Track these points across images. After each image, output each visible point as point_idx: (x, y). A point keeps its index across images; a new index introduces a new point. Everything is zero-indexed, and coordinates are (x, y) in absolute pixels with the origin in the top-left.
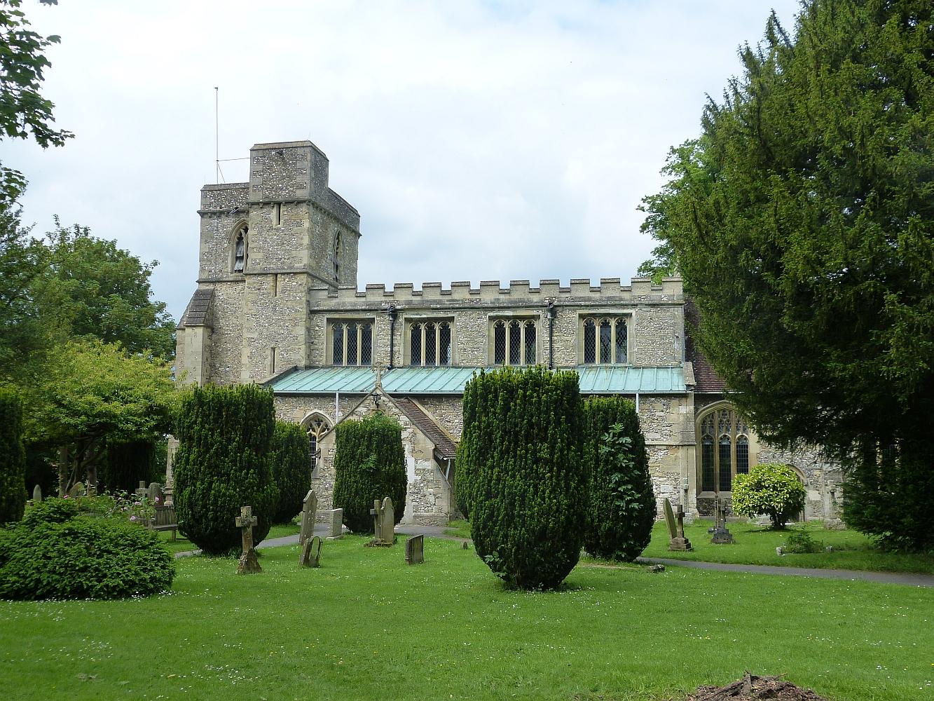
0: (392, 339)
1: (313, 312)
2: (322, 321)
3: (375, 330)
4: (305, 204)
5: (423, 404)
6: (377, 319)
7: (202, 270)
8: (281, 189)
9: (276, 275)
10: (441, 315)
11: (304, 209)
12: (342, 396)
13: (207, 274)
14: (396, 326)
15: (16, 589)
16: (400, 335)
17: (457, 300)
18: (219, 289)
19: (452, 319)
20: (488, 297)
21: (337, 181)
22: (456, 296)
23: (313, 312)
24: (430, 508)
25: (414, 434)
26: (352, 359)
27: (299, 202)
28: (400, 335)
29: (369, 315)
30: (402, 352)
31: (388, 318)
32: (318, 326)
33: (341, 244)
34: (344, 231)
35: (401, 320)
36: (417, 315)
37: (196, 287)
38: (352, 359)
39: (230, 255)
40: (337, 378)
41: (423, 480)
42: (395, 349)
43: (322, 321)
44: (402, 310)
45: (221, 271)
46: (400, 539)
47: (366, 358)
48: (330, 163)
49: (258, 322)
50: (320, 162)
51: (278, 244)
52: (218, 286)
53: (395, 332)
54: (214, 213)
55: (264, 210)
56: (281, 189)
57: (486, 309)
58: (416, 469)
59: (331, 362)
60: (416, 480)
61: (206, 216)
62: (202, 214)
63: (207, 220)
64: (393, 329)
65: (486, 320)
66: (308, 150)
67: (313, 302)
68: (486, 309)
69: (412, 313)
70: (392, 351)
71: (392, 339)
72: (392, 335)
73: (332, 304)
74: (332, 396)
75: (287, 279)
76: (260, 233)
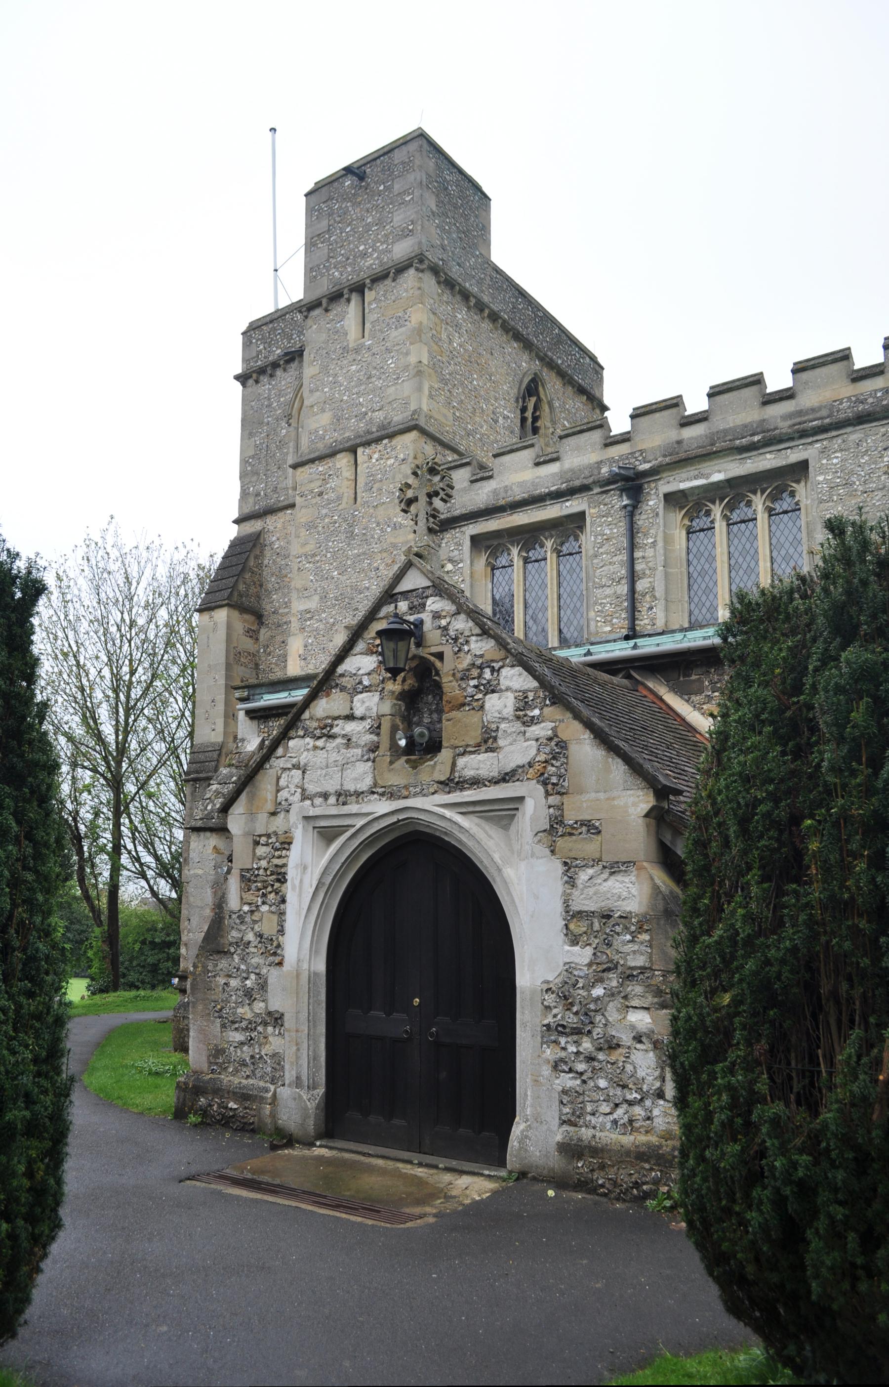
0: (632, 561)
4: (412, 271)
5: (684, 692)
6: (591, 513)
7: (244, 494)
8: (364, 255)
10: (768, 461)
13: (251, 500)
14: (642, 520)
15: (772, 1116)
16: (654, 544)
17: (813, 410)
18: (271, 528)
19: (801, 469)
21: (516, 249)
24: (638, 1110)
25: (558, 748)
27: (401, 269)
28: (654, 544)
29: (572, 506)
30: (660, 592)
31: (619, 501)
32: (450, 560)
33: (546, 407)
34: (552, 386)
35: (653, 502)
36: (696, 478)
37: (233, 531)
39: (291, 450)
41: (603, 968)
42: (641, 586)
45: (275, 490)
48: (605, 373)
49: (318, 571)
50: (461, 200)
51: (360, 383)
52: (271, 522)
53: (640, 539)
55: (331, 315)
56: (364, 255)
58: (572, 915)
60: (569, 968)
61: (251, 382)
62: (243, 378)
64: (632, 533)
66: (413, 147)
69: (684, 476)
70: (632, 591)
71: (632, 561)
72: (632, 546)
73: (483, 495)
75: (376, 456)
76: (325, 369)
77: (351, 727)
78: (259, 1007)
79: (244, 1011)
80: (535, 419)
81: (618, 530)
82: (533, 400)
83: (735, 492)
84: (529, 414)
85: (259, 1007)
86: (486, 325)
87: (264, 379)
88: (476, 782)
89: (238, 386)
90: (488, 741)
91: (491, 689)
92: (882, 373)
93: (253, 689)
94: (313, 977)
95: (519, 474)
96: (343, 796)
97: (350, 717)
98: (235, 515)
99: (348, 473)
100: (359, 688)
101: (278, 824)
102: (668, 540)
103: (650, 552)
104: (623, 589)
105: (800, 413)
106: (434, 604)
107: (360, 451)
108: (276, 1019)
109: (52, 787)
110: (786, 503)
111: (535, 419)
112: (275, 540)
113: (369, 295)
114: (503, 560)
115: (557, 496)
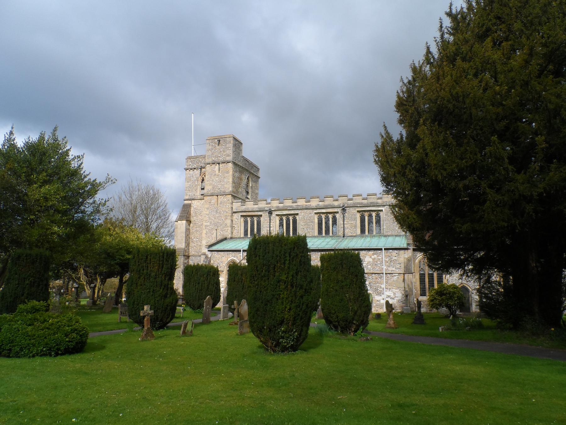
3: (262, 219)
10: (292, 212)
22: (299, 204)
26: (327, 232)
59: (242, 236)
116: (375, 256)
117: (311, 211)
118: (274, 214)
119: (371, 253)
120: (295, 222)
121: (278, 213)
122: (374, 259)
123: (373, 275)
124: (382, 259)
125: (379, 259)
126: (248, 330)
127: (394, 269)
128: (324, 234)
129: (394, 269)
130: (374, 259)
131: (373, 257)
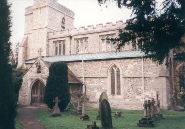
1: (49, 39)
2: (51, 42)
3: (66, 43)
6: (66, 40)
9: (39, 29)
10: (84, 36)
11: (47, 8)
12: (85, 61)
20: (99, 29)
22: (89, 30)
23: (49, 39)
26: (60, 54)
31: (49, 34)
35: (73, 39)
37: (24, 36)
38: (60, 54)
40: (128, 54)
43: (51, 42)
44: (73, 36)
46: (154, 6)
47: (64, 53)
54: (28, 14)
55: (36, 11)
57: (98, 33)
59: (54, 54)
62: (25, 15)
63: (26, 17)
65: (98, 37)
67: (49, 36)
68: (98, 33)
73: (54, 36)
74: (81, 61)
77: (34, 71)
78: (25, 94)
79: (24, 95)
80: (64, 22)
81: (74, 37)
82: (64, 20)
83: (81, 39)
84: (63, 22)
85: (25, 94)
86: (57, 12)
87: (28, 16)
88: (43, 76)
89: (24, 16)
90: (44, 73)
91: (45, 69)
92: (96, 28)
93: (26, 61)
94: (30, 92)
95: (59, 34)
96: (33, 76)
97: (34, 70)
98: (24, 14)
99: (38, 32)
100: (34, 68)
101: (27, 79)
102: (74, 44)
103: (72, 45)
104: (70, 49)
105: (88, 31)
106: (40, 61)
107: (40, 29)
108: (27, 96)
109: (53, 106)
110: (86, 41)
111: (64, 22)
112: (29, 38)
113: (41, 9)
114: (57, 44)
115: (63, 37)
116: (136, 63)
117: (96, 34)
118: (73, 38)
119: (133, 61)
120: (64, 45)
121: (76, 37)
122: (135, 66)
123: (135, 79)
124: (141, 65)
125: (139, 66)
126: (19, 101)
127: (151, 73)
128: (58, 54)
129: (151, 73)
130: (135, 66)
131: (134, 64)
